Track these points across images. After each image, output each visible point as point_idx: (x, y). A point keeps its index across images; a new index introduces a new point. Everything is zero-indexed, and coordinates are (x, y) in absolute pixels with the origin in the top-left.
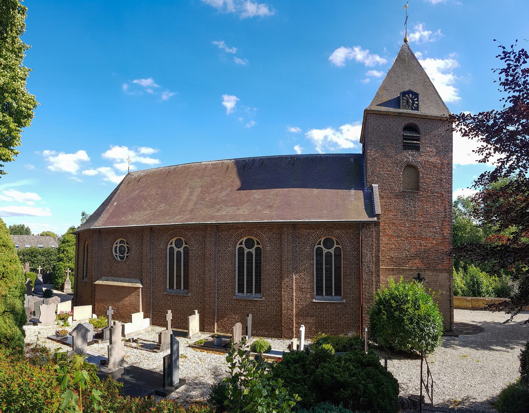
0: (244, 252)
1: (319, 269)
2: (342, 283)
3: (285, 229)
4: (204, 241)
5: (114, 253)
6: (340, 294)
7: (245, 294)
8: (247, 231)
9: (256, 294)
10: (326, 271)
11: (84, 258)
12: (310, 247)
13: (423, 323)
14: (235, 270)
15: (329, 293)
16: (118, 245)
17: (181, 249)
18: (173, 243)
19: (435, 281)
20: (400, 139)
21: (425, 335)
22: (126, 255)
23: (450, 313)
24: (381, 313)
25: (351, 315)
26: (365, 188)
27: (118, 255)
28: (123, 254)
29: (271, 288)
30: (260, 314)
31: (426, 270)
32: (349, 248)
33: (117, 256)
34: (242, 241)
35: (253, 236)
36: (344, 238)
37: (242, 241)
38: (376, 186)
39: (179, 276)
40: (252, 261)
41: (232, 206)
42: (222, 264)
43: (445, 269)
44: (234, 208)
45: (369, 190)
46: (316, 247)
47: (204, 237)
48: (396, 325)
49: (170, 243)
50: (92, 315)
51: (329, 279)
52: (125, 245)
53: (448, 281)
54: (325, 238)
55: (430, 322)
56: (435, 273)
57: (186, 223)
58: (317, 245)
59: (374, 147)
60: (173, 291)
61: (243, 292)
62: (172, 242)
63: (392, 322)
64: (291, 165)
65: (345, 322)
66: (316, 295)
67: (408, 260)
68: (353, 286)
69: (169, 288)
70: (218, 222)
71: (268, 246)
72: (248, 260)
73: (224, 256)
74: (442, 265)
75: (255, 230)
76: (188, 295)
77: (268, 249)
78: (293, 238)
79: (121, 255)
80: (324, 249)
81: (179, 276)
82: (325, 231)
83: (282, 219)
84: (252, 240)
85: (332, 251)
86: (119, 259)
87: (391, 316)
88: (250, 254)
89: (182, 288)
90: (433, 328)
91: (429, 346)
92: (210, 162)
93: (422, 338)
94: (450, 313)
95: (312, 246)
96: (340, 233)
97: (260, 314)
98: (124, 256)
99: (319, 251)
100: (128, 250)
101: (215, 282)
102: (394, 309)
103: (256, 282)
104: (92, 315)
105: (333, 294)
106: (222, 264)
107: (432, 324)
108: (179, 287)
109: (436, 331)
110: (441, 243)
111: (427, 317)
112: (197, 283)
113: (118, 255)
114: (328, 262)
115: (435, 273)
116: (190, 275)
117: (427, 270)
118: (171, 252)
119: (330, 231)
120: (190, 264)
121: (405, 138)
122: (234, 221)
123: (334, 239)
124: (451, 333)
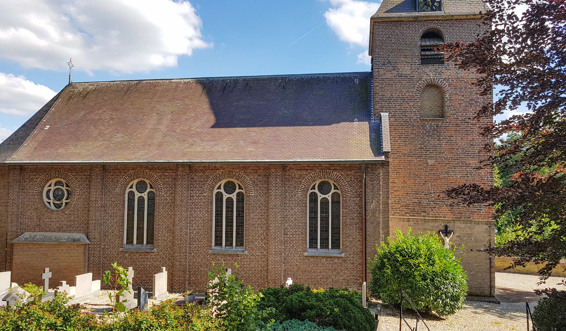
1: (313, 218)
2: (341, 234)
3: (273, 170)
4: (175, 184)
5: (45, 200)
6: (338, 247)
7: (223, 248)
8: (226, 173)
9: (237, 247)
10: (321, 220)
13: (439, 281)
14: (212, 220)
15: (324, 245)
16: (53, 188)
17: (144, 194)
18: (222, 187)
19: (469, 234)
21: (442, 294)
22: (64, 201)
23: (490, 274)
24: (384, 267)
25: (352, 270)
28: (59, 200)
29: (256, 240)
30: (242, 270)
31: (455, 221)
32: (349, 194)
33: (49, 203)
34: (221, 185)
35: (234, 178)
36: (344, 181)
37: (221, 185)
38: (386, 115)
39: (140, 229)
40: (233, 208)
41: (208, 141)
44: (212, 143)
45: (378, 120)
46: (310, 191)
47: (175, 179)
48: (402, 280)
49: (129, 186)
50: (11, 284)
51: (325, 230)
52: (64, 188)
53: (487, 235)
54: (140, 179)
55: (448, 279)
56: (469, 225)
57: (152, 161)
60: (132, 247)
61: (221, 244)
62: (132, 185)
63: (398, 278)
64: (281, 89)
66: (309, 248)
67: (430, 208)
68: (354, 239)
69: (127, 244)
70: (191, 161)
71: (253, 191)
72: (227, 207)
73: (198, 203)
74: (479, 214)
76: (153, 251)
80: (319, 194)
81: (140, 229)
82: (320, 172)
83: (269, 158)
84: (233, 183)
85: (329, 197)
86: (53, 207)
87: (396, 270)
89: (145, 242)
90: (452, 286)
91: (447, 307)
92: (182, 80)
93: (438, 297)
94: (490, 274)
95: (304, 191)
97: (242, 270)
100: (68, 194)
101: (186, 234)
102: (400, 263)
103: (237, 234)
104: (11, 284)
105: (330, 247)
107: (451, 282)
109: (455, 290)
111: (444, 274)
113: (51, 201)
114: (325, 210)
115: (469, 225)
117: (458, 220)
120: (156, 213)
122: (211, 159)
123: (332, 182)
124: (491, 299)
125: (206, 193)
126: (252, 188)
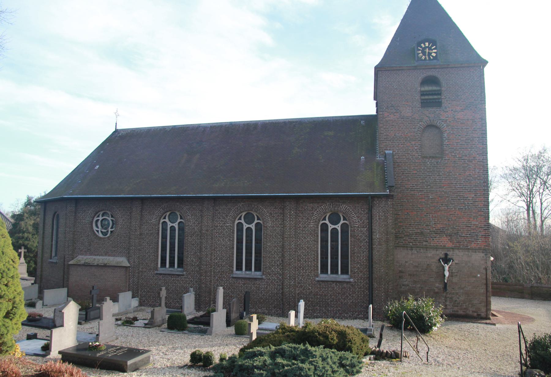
0: (243, 228)
2: (349, 262)
5: (95, 228)
6: (347, 273)
11: (52, 233)
12: (314, 223)
14: (233, 248)
15: (334, 271)
16: (101, 218)
20: (418, 97)
26: (378, 155)
27: (99, 230)
29: (273, 266)
31: (455, 250)
32: (357, 224)
34: (241, 216)
42: (219, 240)
43: (480, 249)
45: (382, 157)
50: (67, 299)
58: (322, 221)
59: (387, 108)
61: (241, 269)
65: (352, 302)
75: (256, 204)
77: (269, 225)
78: (296, 213)
79: (103, 231)
80: (329, 225)
82: (331, 205)
86: (101, 235)
88: (334, 231)
95: (316, 222)
96: (347, 208)
98: (108, 231)
99: (324, 228)
100: (113, 224)
104: (67, 299)
106: (219, 240)
108: (172, 264)
110: (474, 217)
112: (193, 261)
113: (99, 230)
116: (185, 254)
118: (164, 227)
119: (336, 206)
120: (185, 241)
121: (423, 94)
125: (228, 223)
126: (269, 219)
